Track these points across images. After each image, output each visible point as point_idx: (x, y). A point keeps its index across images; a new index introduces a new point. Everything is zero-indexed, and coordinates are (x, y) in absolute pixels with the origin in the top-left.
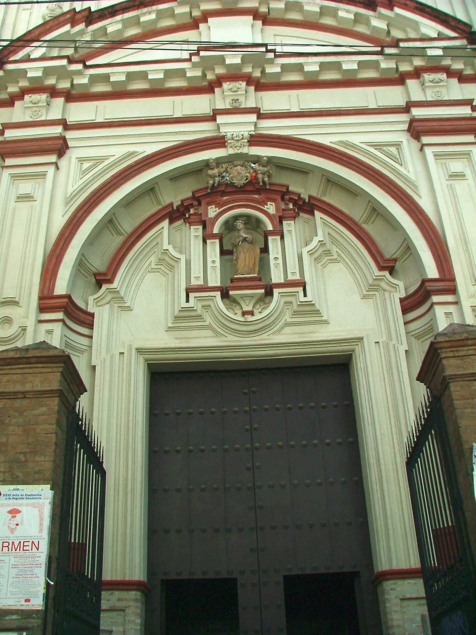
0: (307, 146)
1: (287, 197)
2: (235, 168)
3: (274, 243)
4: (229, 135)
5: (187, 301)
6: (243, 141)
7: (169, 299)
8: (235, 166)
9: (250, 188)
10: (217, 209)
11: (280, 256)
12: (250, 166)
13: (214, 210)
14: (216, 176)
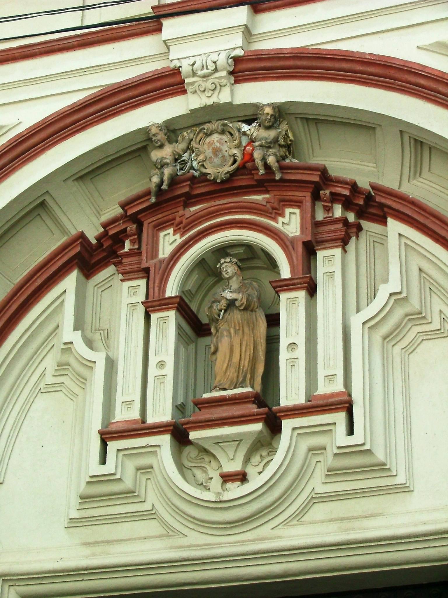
0: (359, 67)
1: (326, 193)
2: (208, 140)
3: (292, 308)
4: (185, 69)
5: (103, 461)
6: (217, 75)
7: (243, 362)
8: (208, 134)
9: (243, 181)
10: (178, 236)
11: (301, 341)
12: (239, 130)
13: (172, 238)
14: (167, 164)
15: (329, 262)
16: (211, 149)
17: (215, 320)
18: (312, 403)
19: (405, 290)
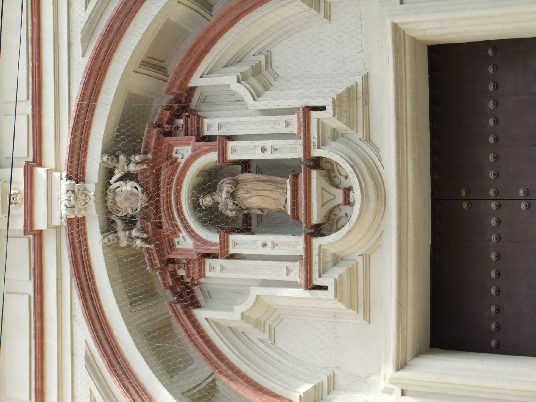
2: (119, 205)
3: (237, 152)
5: (325, 288)
6: (76, 191)
11: (260, 143)
14: (130, 234)
15: (212, 126)
16: (125, 203)
17: (241, 209)
18: (302, 135)
19: (237, 73)
